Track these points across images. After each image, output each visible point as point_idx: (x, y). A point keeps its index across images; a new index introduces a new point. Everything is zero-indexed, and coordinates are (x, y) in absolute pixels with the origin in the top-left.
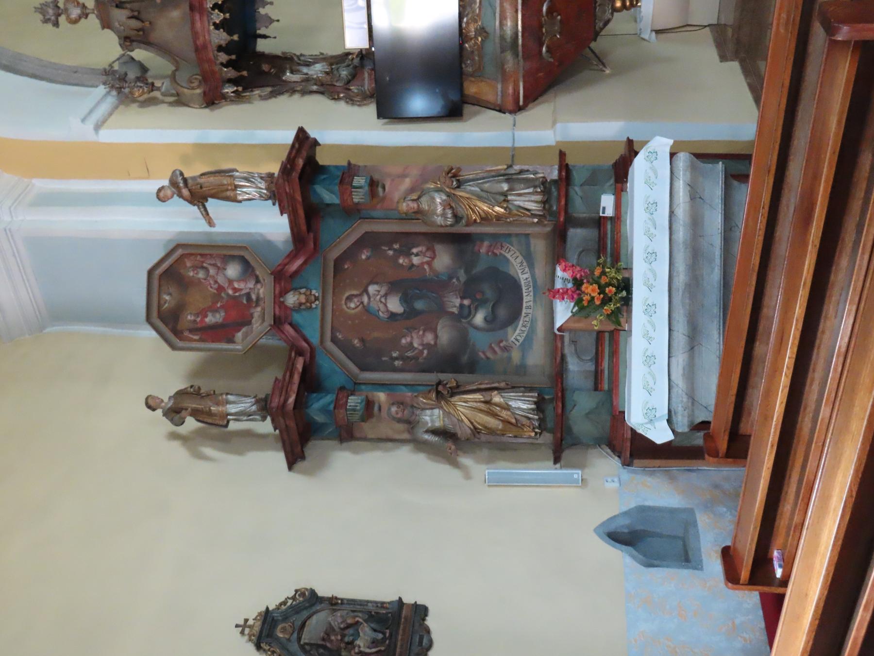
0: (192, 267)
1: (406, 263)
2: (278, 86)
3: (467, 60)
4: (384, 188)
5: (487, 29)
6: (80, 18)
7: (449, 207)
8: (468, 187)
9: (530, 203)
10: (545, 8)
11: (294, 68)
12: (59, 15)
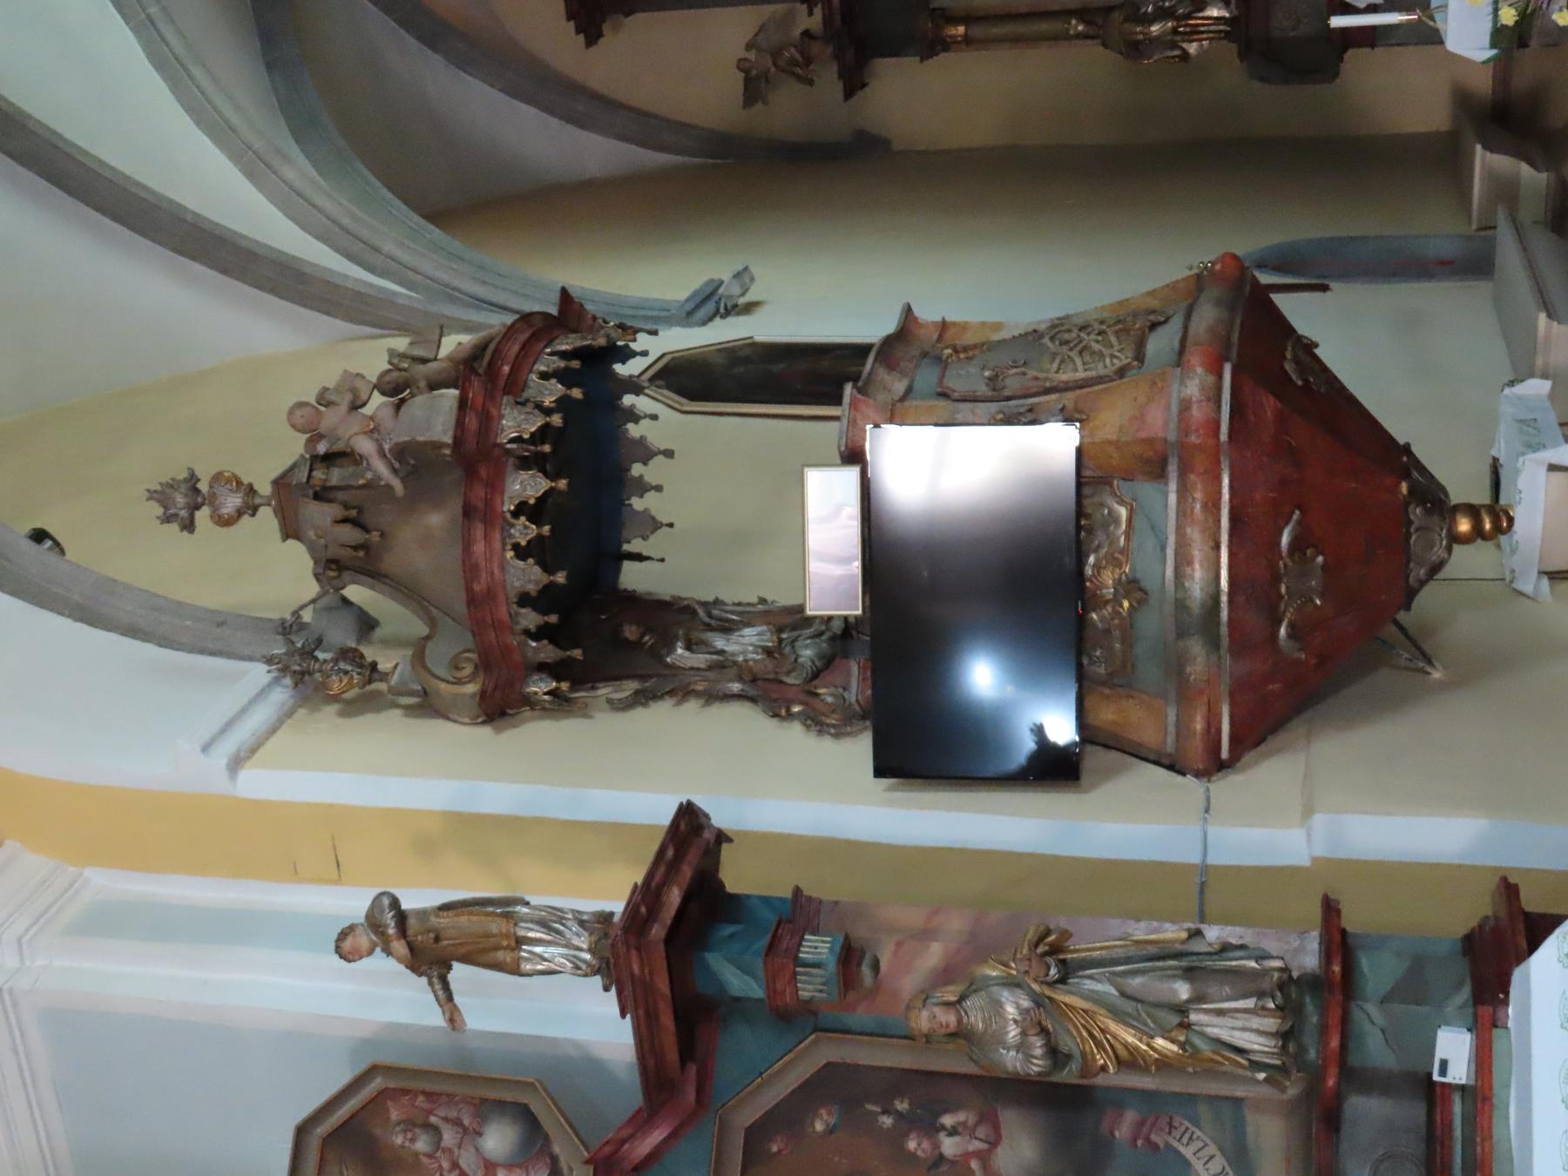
0: (403, 1122)
1: (924, 1151)
2: (654, 679)
3: (1095, 650)
4: (876, 966)
5: (1145, 584)
6: (240, 513)
7: (1038, 1029)
8: (1087, 982)
9: (1247, 1035)
10: (1285, 540)
11: (695, 635)
12: (198, 507)
